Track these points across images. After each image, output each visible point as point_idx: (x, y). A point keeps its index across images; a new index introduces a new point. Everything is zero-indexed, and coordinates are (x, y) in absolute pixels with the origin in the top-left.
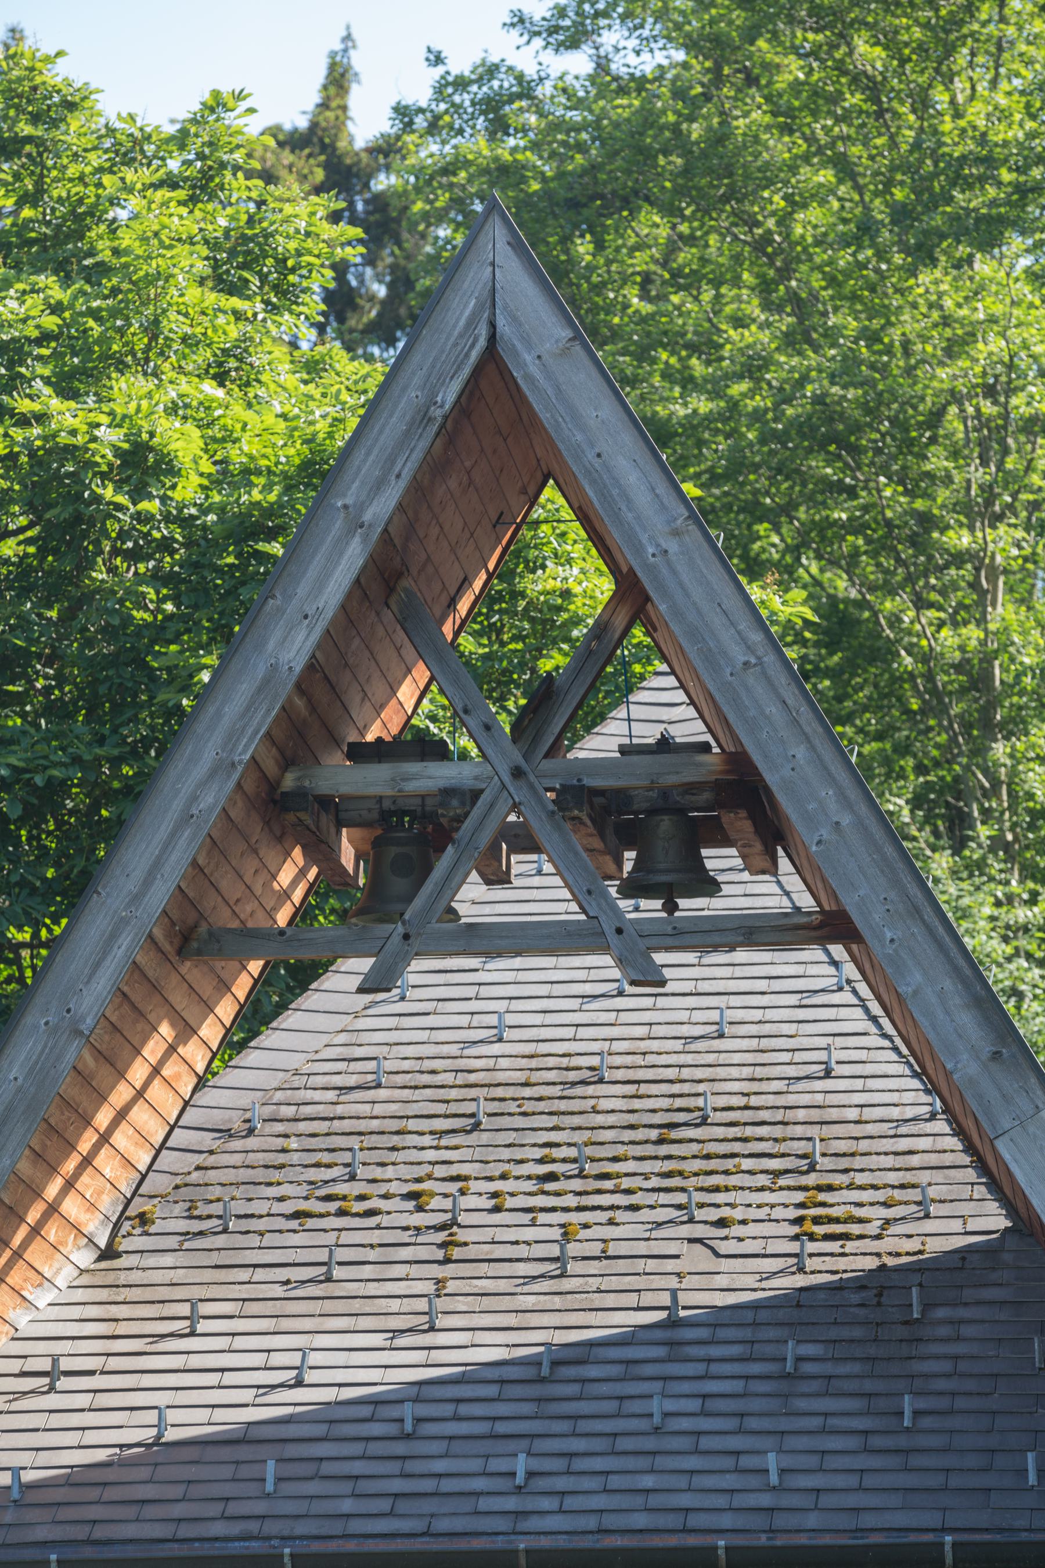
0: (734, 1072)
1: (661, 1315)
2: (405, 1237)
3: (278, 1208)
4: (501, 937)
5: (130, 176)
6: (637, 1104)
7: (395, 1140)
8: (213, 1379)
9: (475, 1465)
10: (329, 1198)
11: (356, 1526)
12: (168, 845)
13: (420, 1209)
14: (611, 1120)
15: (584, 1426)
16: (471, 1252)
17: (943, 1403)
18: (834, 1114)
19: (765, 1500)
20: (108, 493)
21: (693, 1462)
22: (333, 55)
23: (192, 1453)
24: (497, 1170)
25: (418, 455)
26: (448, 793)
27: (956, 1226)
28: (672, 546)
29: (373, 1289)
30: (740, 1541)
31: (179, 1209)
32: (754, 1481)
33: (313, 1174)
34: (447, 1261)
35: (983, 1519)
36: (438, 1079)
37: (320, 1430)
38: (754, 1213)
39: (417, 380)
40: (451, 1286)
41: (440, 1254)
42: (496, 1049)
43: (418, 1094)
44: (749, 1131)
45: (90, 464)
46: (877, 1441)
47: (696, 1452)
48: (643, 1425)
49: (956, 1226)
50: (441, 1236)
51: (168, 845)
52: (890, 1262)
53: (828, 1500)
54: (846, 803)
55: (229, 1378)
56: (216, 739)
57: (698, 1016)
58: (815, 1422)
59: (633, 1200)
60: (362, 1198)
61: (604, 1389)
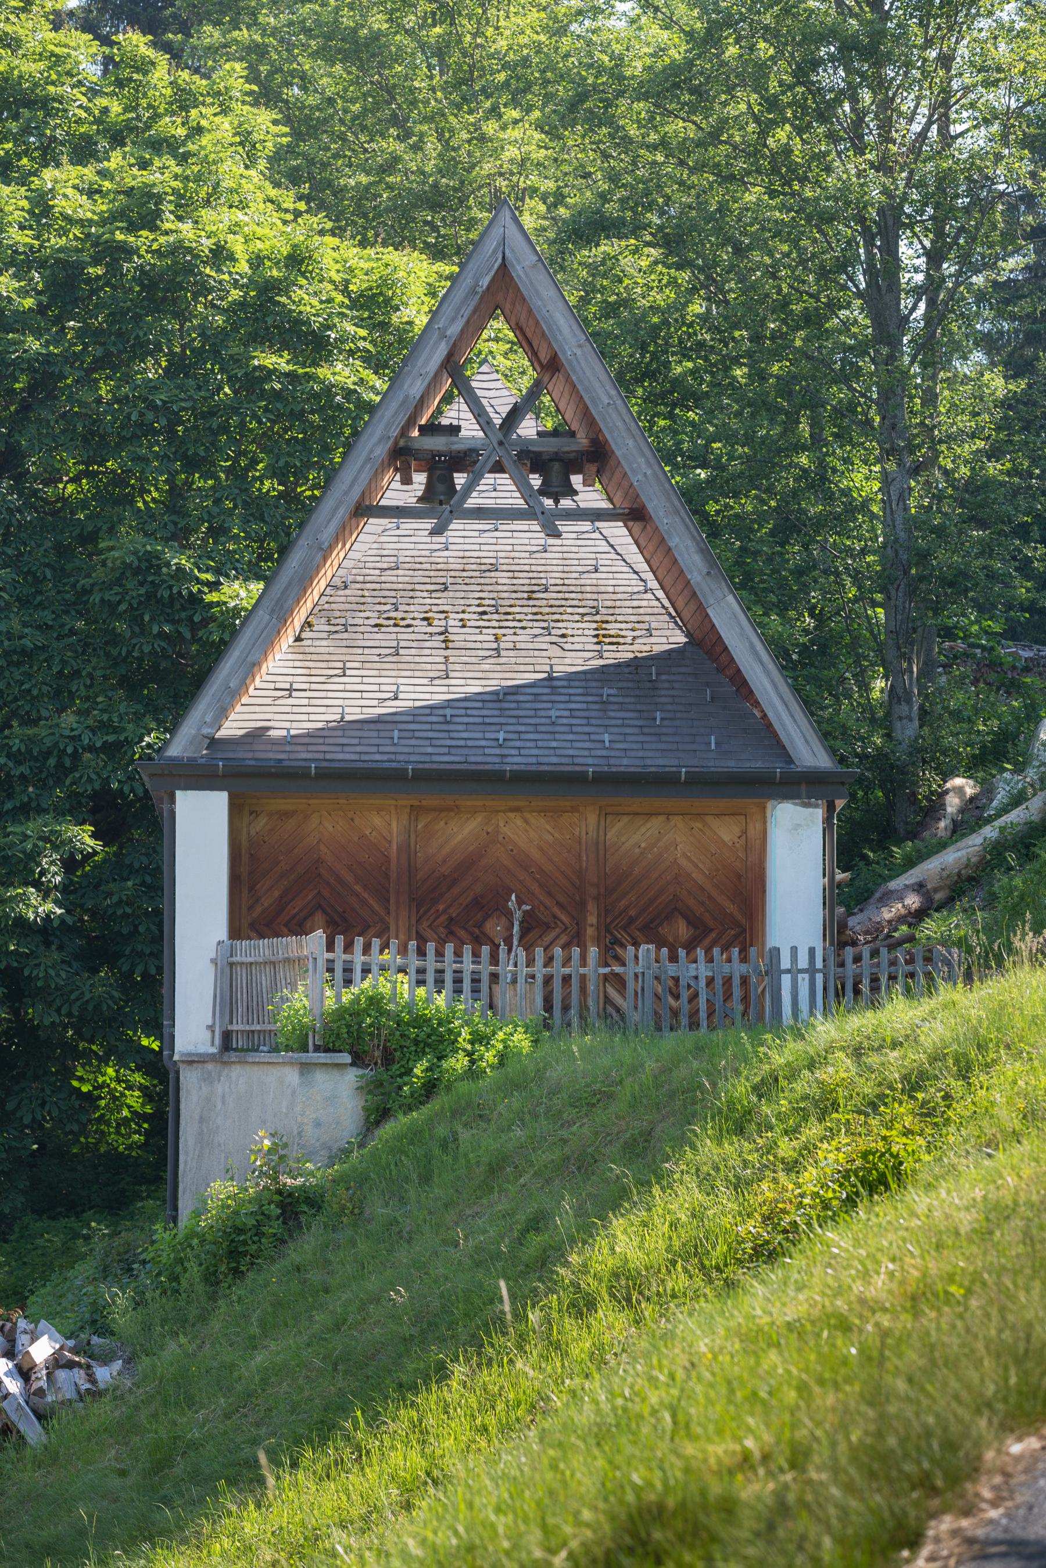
0: (555, 568)
1: (545, 675)
2: (426, 637)
3: (367, 622)
5: (204, 111)
6: (515, 581)
7: (411, 594)
9: (480, 735)
10: (388, 618)
13: (430, 625)
14: (505, 588)
15: (522, 721)
16: (457, 645)
18: (603, 589)
19: (604, 753)
20: (208, 271)
21: (571, 737)
23: (358, 726)
25: (471, 308)
27: (664, 640)
28: (579, 352)
29: (417, 660)
30: (598, 769)
31: (323, 621)
32: (598, 745)
34: (447, 648)
35: (695, 762)
36: (424, 566)
37: (410, 718)
38: (575, 632)
39: (471, 275)
40: (451, 659)
41: (443, 645)
42: (446, 554)
43: (417, 573)
44: (567, 595)
46: (646, 730)
47: (572, 732)
48: (547, 721)
49: (664, 640)
50: (442, 638)
52: (639, 655)
53: (630, 754)
54: (650, 466)
55: (365, 695)
56: (382, 425)
57: (533, 542)
58: (619, 722)
60: (403, 619)
61: (528, 705)
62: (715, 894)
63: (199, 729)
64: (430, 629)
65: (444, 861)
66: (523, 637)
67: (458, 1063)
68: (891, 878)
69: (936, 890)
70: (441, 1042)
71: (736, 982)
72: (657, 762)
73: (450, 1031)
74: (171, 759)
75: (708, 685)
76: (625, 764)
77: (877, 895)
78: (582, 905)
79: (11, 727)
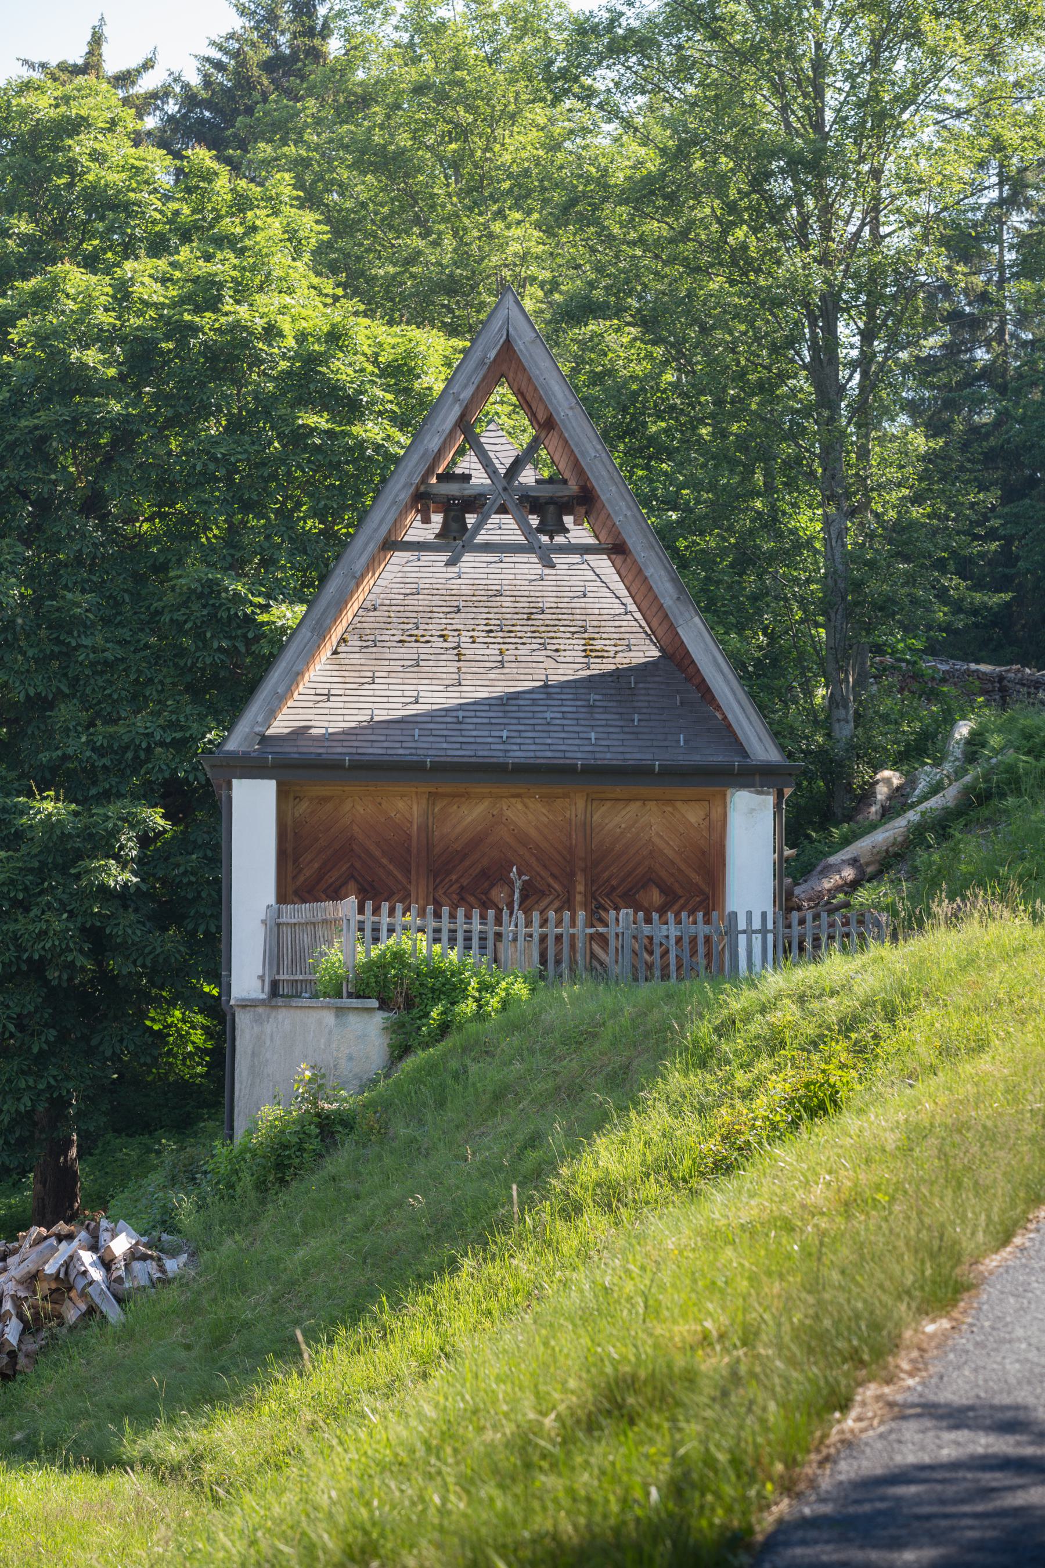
4: (570, 838)
5: (258, 212)
8: (385, 699)
9: (487, 733)
11: (450, 753)
16: (468, 658)
18: (590, 611)
19: (590, 748)
21: (563, 735)
22: (94, 28)
24: (471, 627)
27: (641, 654)
28: (570, 413)
29: (434, 670)
32: (586, 742)
33: (402, 626)
37: (429, 719)
42: (459, 581)
45: (252, 333)
46: (627, 730)
48: (543, 721)
49: (641, 654)
54: (629, 508)
55: (391, 699)
56: (406, 473)
59: (524, 640)
62: (683, 867)
63: (252, 728)
64: (445, 645)
65: (457, 839)
66: (523, 651)
67: (468, 1007)
68: (831, 854)
69: (868, 864)
70: (454, 990)
71: (701, 940)
72: (634, 756)
73: (461, 981)
74: (229, 752)
75: (678, 692)
76: (609, 757)
77: (819, 868)
78: (572, 875)
79: (95, 725)
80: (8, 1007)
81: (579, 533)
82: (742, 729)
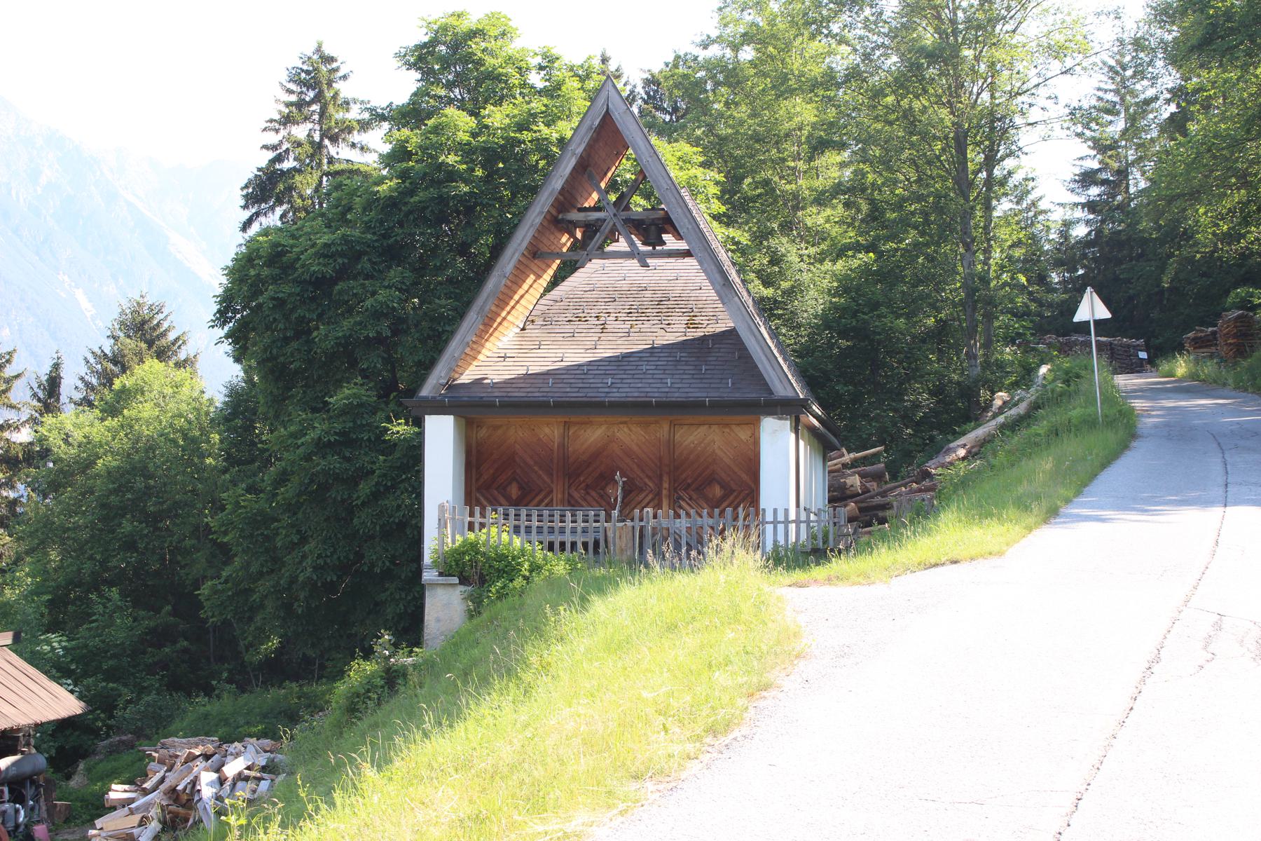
11: (569, 395)
12: (527, 232)
17: (712, 367)
19: (667, 390)
20: (554, 149)
26: (598, 220)
35: (716, 395)
51: (527, 232)
62: (736, 470)
66: (647, 325)
69: (972, 447)
70: (513, 570)
73: (519, 564)
74: (423, 397)
76: (676, 396)
80: (387, 550)
81: (670, 242)
82: (769, 375)
